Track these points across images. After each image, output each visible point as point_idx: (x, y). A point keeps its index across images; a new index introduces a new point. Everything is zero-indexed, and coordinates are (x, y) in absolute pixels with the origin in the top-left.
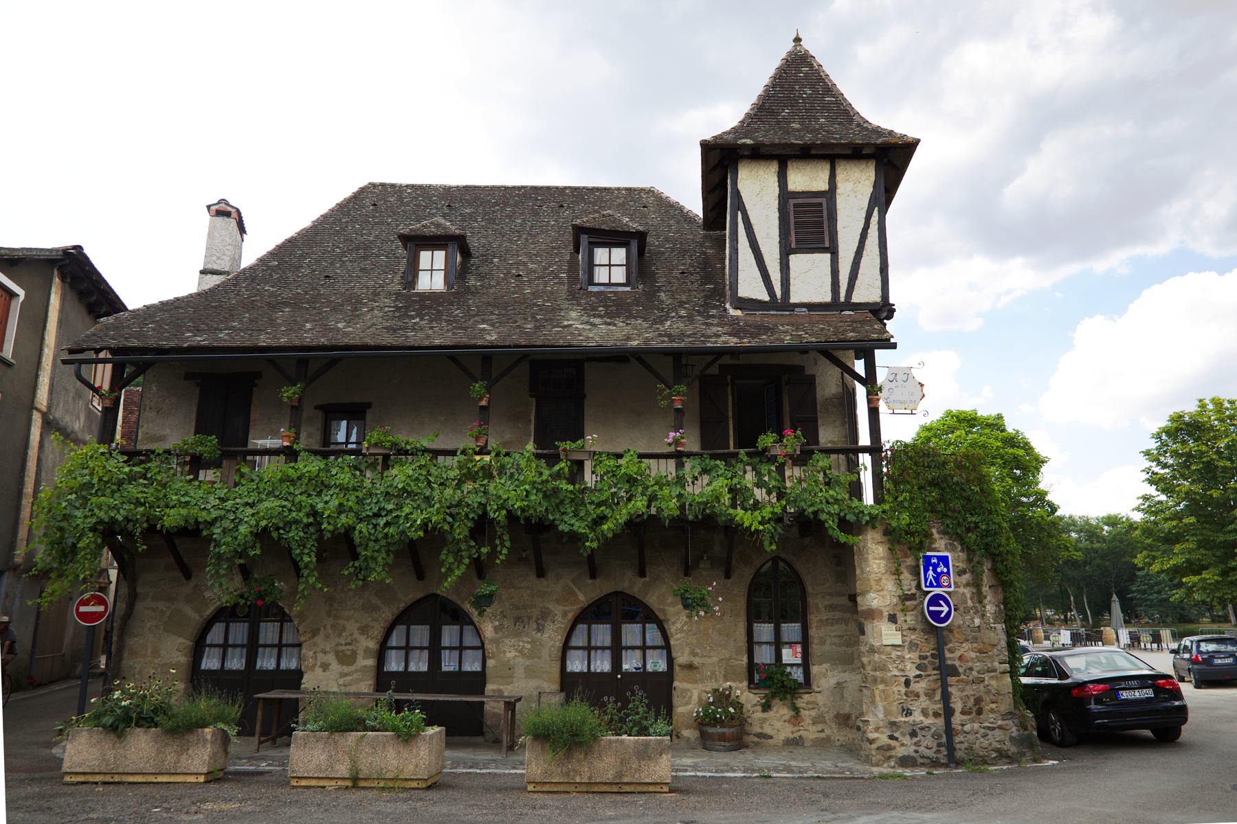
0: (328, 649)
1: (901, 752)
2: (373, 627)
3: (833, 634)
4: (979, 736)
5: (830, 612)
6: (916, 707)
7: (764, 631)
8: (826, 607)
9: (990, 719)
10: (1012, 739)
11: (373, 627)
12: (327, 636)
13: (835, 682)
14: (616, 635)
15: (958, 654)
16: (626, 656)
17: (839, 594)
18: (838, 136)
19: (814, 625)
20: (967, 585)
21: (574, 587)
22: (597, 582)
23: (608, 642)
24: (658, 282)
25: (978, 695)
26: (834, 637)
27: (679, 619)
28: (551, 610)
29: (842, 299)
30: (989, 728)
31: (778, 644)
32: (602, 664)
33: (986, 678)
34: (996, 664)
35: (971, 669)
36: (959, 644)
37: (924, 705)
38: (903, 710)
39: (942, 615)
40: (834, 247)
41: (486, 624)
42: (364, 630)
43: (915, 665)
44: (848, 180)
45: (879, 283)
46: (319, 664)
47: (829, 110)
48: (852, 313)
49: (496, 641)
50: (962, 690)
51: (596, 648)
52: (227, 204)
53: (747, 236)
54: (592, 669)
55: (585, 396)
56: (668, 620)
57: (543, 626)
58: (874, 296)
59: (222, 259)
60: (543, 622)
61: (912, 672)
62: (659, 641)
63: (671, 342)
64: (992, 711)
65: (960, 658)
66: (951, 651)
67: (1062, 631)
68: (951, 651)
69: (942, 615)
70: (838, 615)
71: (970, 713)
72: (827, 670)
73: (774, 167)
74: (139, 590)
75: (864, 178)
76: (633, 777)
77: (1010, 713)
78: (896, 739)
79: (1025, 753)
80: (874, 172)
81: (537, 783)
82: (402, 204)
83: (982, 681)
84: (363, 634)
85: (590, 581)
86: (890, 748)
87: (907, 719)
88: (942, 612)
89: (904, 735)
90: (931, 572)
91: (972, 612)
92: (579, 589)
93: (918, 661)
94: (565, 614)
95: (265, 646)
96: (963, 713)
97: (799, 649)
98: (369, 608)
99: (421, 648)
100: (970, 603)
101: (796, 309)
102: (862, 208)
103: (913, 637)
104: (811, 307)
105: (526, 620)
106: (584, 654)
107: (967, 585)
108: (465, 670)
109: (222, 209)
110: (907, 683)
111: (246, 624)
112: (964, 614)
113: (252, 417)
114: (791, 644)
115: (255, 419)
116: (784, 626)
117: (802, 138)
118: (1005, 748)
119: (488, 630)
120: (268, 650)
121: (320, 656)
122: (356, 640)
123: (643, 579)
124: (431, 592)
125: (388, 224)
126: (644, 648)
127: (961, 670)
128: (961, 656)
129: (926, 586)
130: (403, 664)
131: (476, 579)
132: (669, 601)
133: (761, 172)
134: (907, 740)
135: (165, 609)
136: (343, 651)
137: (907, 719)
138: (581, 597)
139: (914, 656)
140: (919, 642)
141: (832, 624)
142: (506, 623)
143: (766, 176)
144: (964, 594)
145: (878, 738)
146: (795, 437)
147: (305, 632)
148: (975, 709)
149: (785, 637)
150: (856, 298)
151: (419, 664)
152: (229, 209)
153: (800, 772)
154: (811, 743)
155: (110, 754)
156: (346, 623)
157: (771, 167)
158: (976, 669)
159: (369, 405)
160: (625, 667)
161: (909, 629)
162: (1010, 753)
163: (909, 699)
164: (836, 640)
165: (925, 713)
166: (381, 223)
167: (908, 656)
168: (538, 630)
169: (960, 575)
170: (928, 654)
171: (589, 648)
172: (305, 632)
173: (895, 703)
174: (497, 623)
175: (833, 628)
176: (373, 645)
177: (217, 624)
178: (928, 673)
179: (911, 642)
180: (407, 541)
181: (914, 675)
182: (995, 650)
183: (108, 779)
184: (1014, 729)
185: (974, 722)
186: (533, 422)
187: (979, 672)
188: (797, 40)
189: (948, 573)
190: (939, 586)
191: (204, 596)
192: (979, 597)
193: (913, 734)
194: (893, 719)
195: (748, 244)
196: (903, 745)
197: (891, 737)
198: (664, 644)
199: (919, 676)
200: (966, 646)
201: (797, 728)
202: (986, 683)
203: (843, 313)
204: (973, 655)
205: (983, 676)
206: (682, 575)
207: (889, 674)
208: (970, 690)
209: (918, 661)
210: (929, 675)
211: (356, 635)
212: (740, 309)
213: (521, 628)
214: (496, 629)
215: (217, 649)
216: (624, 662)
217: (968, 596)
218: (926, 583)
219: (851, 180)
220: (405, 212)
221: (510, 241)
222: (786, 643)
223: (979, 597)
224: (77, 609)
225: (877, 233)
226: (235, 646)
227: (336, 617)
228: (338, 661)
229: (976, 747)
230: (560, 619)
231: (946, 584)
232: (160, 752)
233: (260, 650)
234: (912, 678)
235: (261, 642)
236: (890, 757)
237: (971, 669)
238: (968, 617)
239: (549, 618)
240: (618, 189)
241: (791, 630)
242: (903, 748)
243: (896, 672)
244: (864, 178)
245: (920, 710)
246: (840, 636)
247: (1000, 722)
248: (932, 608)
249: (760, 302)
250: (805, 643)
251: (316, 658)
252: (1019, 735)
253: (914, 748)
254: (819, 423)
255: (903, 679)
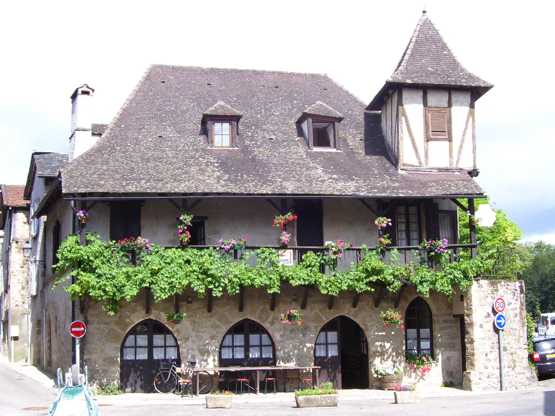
0: (194, 348)
5: (444, 323)
7: (412, 332)
8: (442, 321)
11: (217, 336)
12: (194, 342)
13: (446, 357)
14: (247, 340)
17: (449, 315)
19: (437, 330)
22: (332, 310)
23: (243, 343)
26: (446, 335)
27: (373, 329)
28: (309, 326)
31: (419, 339)
33: (518, 352)
36: (507, 337)
38: (485, 367)
40: (450, 138)
41: (276, 334)
44: (457, 102)
52: (88, 87)
54: (235, 357)
55: (323, 214)
56: (367, 329)
57: (306, 334)
66: (504, 340)
68: (504, 340)
70: (448, 324)
73: (421, 94)
74: (89, 318)
75: (465, 101)
80: (470, 98)
85: (328, 311)
88: (501, 323)
105: (296, 331)
106: (258, 348)
108: (224, 358)
110: (486, 355)
111: (408, 330)
113: (142, 224)
115: (144, 225)
121: (191, 352)
123: (354, 309)
124: (246, 318)
131: (269, 311)
132: (368, 320)
133: (414, 96)
135: (105, 329)
136: (202, 349)
138: (324, 318)
139: (490, 343)
140: (492, 336)
141: (445, 329)
142: (286, 333)
143: (417, 98)
146: (492, 241)
149: (422, 336)
151: (240, 355)
156: (203, 334)
157: (419, 93)
159: (206, 218)
163: (487, 362)
164: (447, 337)
174: (282, 333)
175: (446, 331)
180: (208, 289)
186: (296, 227)
191: (125, 322)
199: (491, 352)
200: (511, 337)
206: (374, 306)
214: (281, 335)
215: (258, 347)
219: (459, 102)
226: (331, 344)
227: (197, 331)
228: (200, 354)
237: (512, 348)
241: (425, 332)
246: (449, 335)
250: (431, 339)
251: (188, 353)
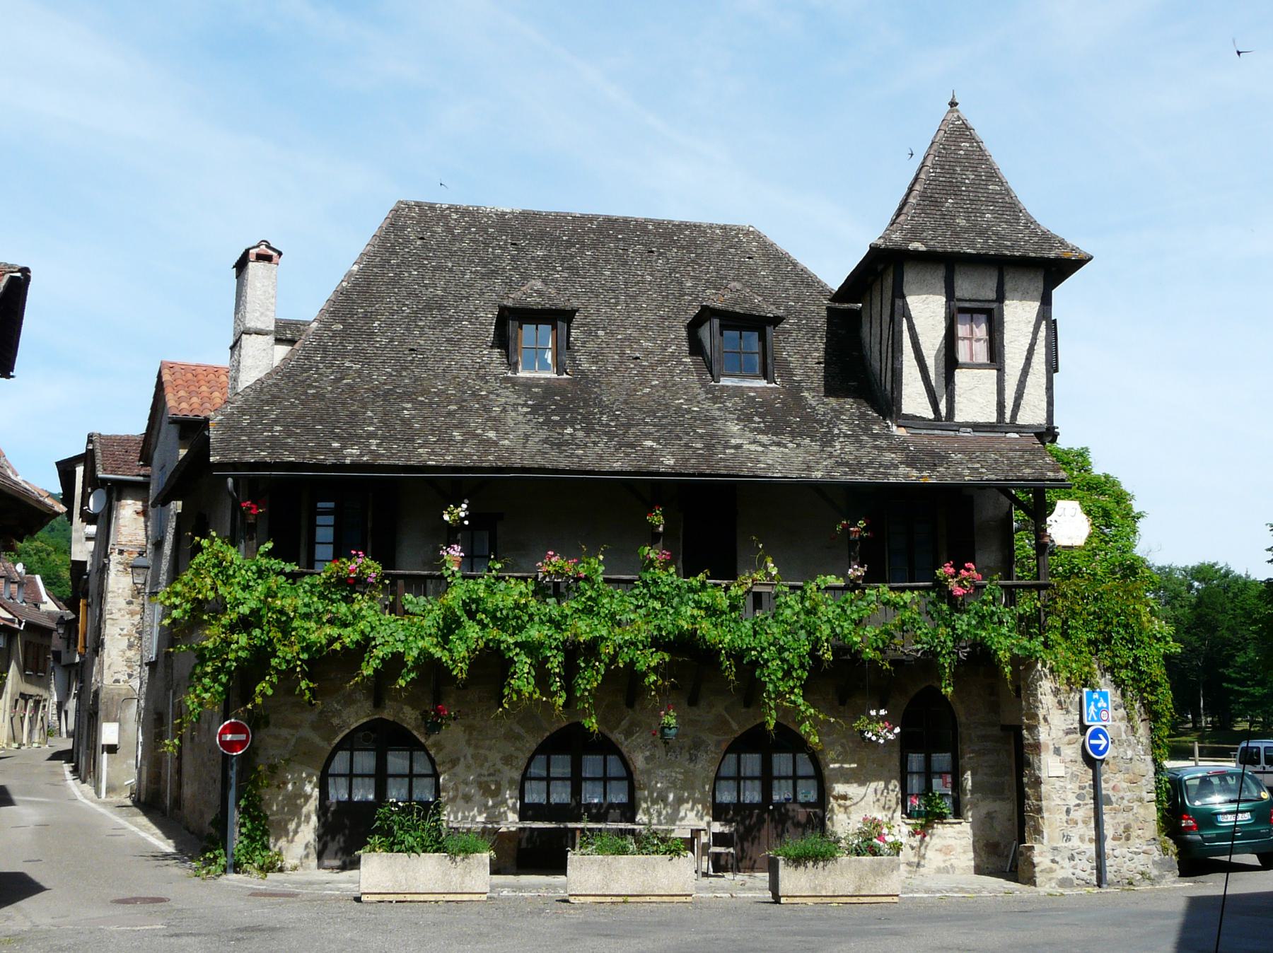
1: (1061, 874)
2: (517, 758)
3: (986, 764)
4: (1126, 859)
6: (1075, 833)
9: (1137, 844)
10: (1154, 863)
12: (468, 767)
15: (1111, 784)
16: (744, 786)
18: (1009, 243)
20: (1122, 719)
21: (727, 716)
24: (795, 375)
25: (1127, 822)
29: (1008, 420)
30: (1136, 853)
32: (752, 795)
33: (1135, 807)
34: (1144, 794)
35: (1122, 798)
36: (1113, 775)
37: (1081, 832)
38: (1064, 836)
39: (1101, 748)
41: (636, 754)
42: (508, 760)
43: (1075, 795)
45: (1044, 405)
46: (460, 795)
47: (994, 203)
48: (1017, 436)
49: (648, 772)
50: (1114, 818)
51: (746, 778)
52: (268, 247)
53: (913, 347)
57: (696, 756)
58: (1039, 418)
59: (266, 316)
60: (696, 752)
61: (1073, 801)
62: (623, 773)
63: (854, 473)
64: (1139, 837)
65: (1114, 788)
67: (492, 701)
68: (1106, 782)
69: (1101, 748)
71: (1120, 839)
72: (978, 800)
76: (870, 890)
77: (1154, 839)
78: (1057, 863)
79: (1164, 875)
81: (788, 896)
82: (455, 239)
83: (1131, 810)
84: (507, 765)
85: (743, 710)
86: (1051, 870)
87: (1066, 845)
88: (1100, 745)
89: (1063, 859)
90: (1092, 707)
91: (1125, 744)
92: (732, 718)
93: (1078, 791)
94: (718, 744)
95: (780, 778)
96: (1114, 839)
97: (949, 779)
98: (511, 737)
99: (752, 778)
100: (1124, 737)
101: (961, 429)
102: (1030, 322)
103: (1074, 769)
104: (976, 427)
105: (678, 750)
107: (1122, 719)
109: (262, 252)
110: (1068, 811)
112: (1118, 747)
114: (941, 774)
116: (935, 756)
117: (972, 244)
118: (1148, 871)
119: (639, 761)
120: (783, 782)
122: (499, 771)
125: (451, 270)
126: (795, 778)
127: (1113, 799)
128: (1114, 787)
129: (1088, 721)
130: (735, 794)
134: (1066, 863)
135: (289, 737)
137: (1066, 845)
138: (735, 726)
142: (657, 753)
143: (933, 281)
144: (1119, 728)
145: (1041, 862)
147: (444, 762)
148: (1124, 835)
150: (1021, 420)
152: (270, 252)
153: (976, 893)
154: (962, 871)
155: (402, 876)
156: (487, 753)
158: (1126, 798)
160: (776, 798)
161: (1071, 761)
162: (1152, 876)
163: (1069, 826)
165: (1082, 839)
166: (439, 268)
167: (1069, 787)
168: (691, 760)
169: (1116, 710)
170: (1087, 784)
171: (351, 776)
172: (444, 762)
173: (1058, 830)
174: (648, 753)
176: (517, 775)
177: (340, 752)
178: (1086, 802)
179: (1072, 773)
181: (1074, 804)
182: (1144, 781)
183: (401, 898)
184: (1157, 853)
185: (1122, 847)
187: (1129, 801)
188: (953, 104)
189: (1107, 707)
190: (1100, 719)
192: (1133, 729)
193: (1072, 858)
194: (1055, 845)
195: (913, 355)
196: (1062, 868)
197: (1053, 861)
198: (625, 775)
199: (1078, 805)
200: (1120, 776)
201: (948, 857)
202: (1135, 811)
203: (1008, 435)
204: (1125, 785)
205: (1132, 805)
207: (1053, 803)
208: (1121, 818)
209: (1078, 791)
210: (1086, 804)
211: (499, 765)
212: (904, 427)
213: (673, 759)
214: (646, 758)
215: (343, 779)
216: (774, 793)
217: (1123, 728)
218: (1088, 717)
220: (464, 252)
221: (608, 303)
222: (936, 773)
223: (1133, 729)
224: (248, 737)
225: (1044, 350)
227: (476, 747)
229: (1124, 870)
230: (713, 749)
231: (1105, 719)
232: (446, 874)
233: (776, 783)
234: (1072, 807)
235: (776, 773)
236: (1050, 879)
237: (1122, 798)
238: (1122, 750)
239: (702, 748)
240: (711, 227)
241: (942, 760)
242: (1063, 870)
243: (1059, 802)
244: (1032, 288)
245: (1078, 836)
247: (1145, 848)
248: (1093, 742)
249: (923, 419)
252: (1161, 859)
253: (1072, 870)
254: (976, 547)
255: (1065, 808)
